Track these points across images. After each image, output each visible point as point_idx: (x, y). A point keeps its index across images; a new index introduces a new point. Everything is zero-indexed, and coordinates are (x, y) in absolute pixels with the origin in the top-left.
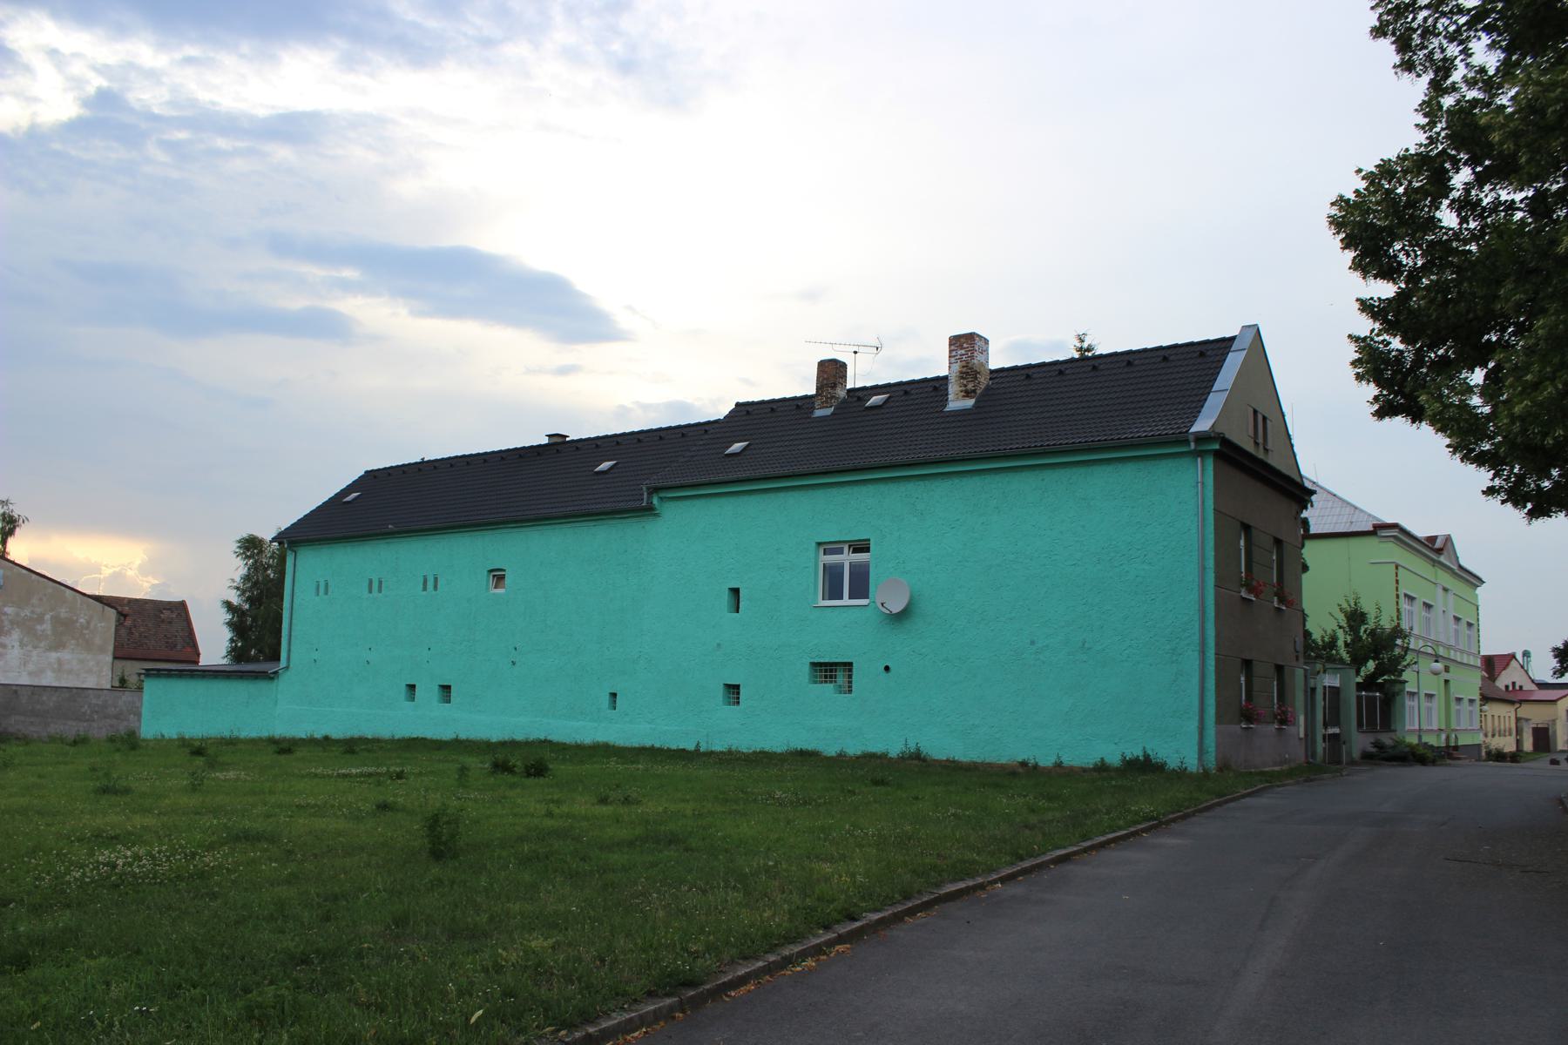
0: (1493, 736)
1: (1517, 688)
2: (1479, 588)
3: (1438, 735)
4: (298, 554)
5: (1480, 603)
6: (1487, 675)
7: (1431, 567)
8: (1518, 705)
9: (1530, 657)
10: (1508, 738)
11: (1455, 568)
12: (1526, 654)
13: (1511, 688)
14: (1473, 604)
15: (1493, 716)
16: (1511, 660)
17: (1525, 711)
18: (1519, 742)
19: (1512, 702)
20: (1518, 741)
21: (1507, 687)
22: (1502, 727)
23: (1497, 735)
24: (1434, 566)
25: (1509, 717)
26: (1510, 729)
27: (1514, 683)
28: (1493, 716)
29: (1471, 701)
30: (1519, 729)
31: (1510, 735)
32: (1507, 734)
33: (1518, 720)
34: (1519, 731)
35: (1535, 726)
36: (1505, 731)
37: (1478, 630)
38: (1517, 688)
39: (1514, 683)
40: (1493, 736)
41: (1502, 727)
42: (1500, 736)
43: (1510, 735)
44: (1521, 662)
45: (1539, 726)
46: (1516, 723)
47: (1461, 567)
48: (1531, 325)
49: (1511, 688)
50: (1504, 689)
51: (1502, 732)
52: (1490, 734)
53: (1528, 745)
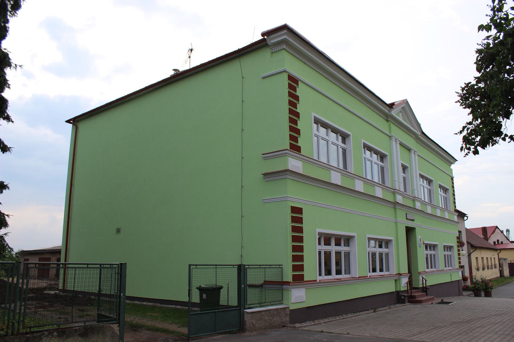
0: (483, 269)
1: (500, 243)
2: (452, 165)
3: (396, 280)
4: (476, 251)
5: (454, 175)
6: (483, 237)
7: (385, 122)
8: (499, 251)
9: (509, 232)
10: (494, 270)
11: (419, 133)
12: (508, 231)
13: (497, 243)
14: (451, 176)
15: (482, 258)
16: (496, 229)
17: (503, 255)
18: (501, 272)
19: (496, 250)
20: (500, 271)
21: (494, 242)
22: (490, 264)
23: (486, 268)
24: (387, 121)
25: (494, 258)
26: (495, 265)
27: (498, 241)
28: (482, 258)
29: (449, 248)
30: (501, 264)
31: (495, 267)
32: (493, 267)
33: (499, 259)
34: (501, 266)
35: (510, 262)
36: (492, 266)
37: (454, 195)
38: (500, 243)
39: (498, 241)
40: (483, 269)
41: (490, 264)
42: (488, 268)
43: (495, 267)
44: (506, 236)
45: (512, 262)
46: (499, 261)
47: (423, 133)
48: (497, 82)
49: (497, 243)
50: (493, 244)
51: (490, 267)
52: (481, 269)
53: (506, 273)
